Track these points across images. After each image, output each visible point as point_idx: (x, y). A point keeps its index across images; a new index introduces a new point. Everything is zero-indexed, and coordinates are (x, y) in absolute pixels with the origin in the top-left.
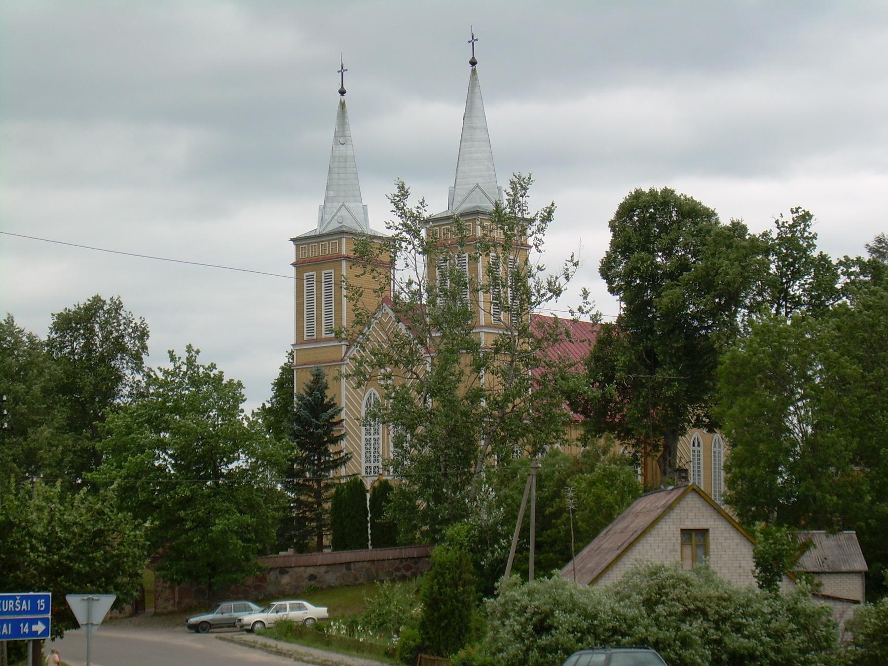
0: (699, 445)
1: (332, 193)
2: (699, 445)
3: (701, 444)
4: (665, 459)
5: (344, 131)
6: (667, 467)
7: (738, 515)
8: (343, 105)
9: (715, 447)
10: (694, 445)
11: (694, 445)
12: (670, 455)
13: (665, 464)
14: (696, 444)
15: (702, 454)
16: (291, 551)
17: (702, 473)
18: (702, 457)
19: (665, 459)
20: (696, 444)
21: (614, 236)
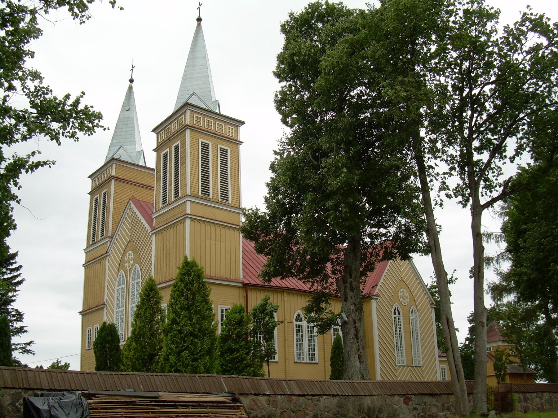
0: (399, 314)
1: (115, 141)
2: (399, 314)
3: (401, 313)
4: (345, 282)
5: (129, 103)
6: (348, 291)
7: (474, 11)
8: (130, 88)
9: (415, 357)
10: (395, 313)
11: (395, 313)
12: (351, 277)
13: (346, 287)
14: (397, 313)
15: (402, 320)
16: (493, 383)
17: (403, 336)
18: (402, 323)
19: (345, 282)
20: (397, 313)
21: (288, 41)
